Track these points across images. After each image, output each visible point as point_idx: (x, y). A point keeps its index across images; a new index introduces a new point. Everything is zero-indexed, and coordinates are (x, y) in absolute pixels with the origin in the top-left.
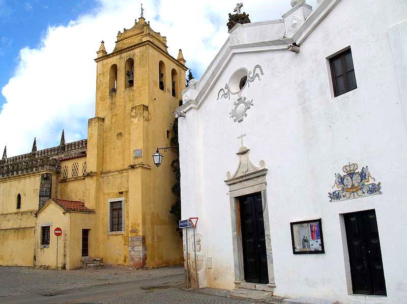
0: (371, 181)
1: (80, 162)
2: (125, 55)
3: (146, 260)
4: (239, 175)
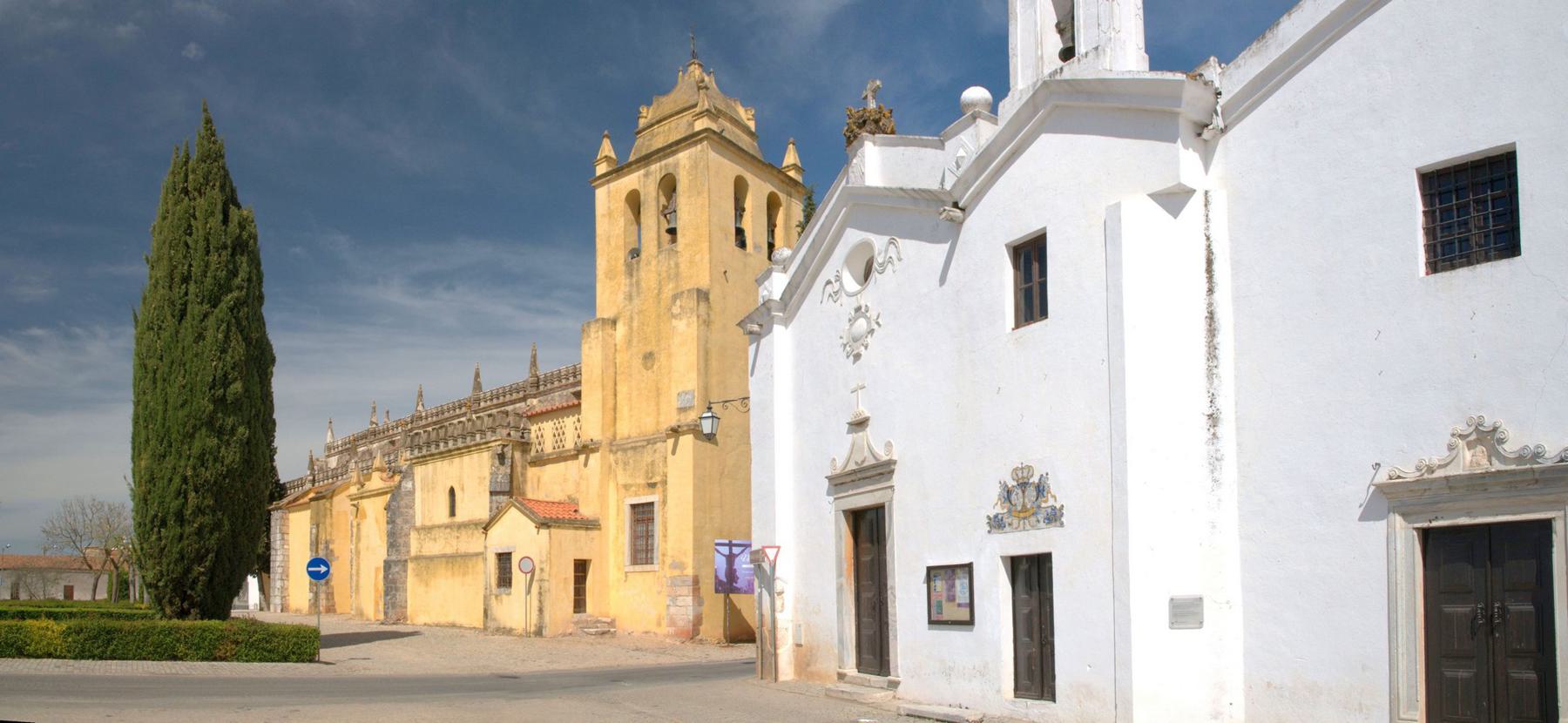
0: (1051, 502)
1: (569, 422)
2: (657, 169)
3: (701, 625)
4: (852, 466)
